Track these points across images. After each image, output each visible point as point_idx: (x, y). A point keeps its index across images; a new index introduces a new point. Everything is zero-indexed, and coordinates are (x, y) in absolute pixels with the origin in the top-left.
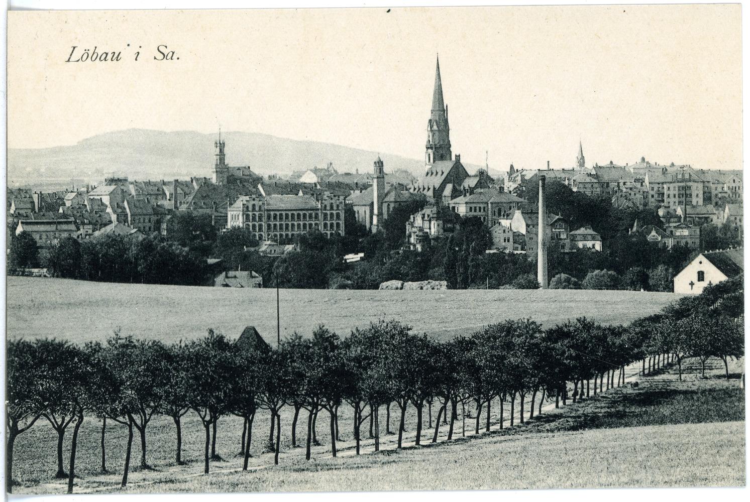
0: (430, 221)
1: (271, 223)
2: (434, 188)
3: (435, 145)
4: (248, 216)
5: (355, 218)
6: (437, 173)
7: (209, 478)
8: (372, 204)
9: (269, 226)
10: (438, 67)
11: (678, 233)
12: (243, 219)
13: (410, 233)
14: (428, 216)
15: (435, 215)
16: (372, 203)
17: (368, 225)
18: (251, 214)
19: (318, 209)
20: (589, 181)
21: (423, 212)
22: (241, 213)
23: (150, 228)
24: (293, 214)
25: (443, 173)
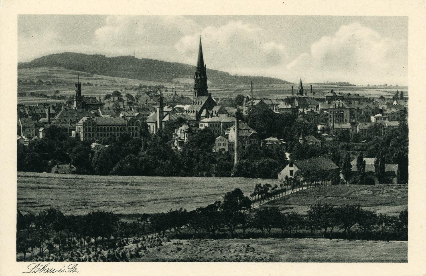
0: (184, 133)
1: (99, 132)
2: (197, 111)
3: (198, 87)
4: (86, 128)
5: (148, 129)
6: (199, 103)
7: (292, 85)
8: (156, 123)
9: (98, 134)
10: (201, 41)
11: (237, 86)
12: (83, 130)
13: (174, 140)
14: (184, 130)
15: (187, 130)
16: (157, 122)
17: (201, 121)
18: (88, 127)
19: (125, 125)
20: (286, 108)
21: (181, 128)
22: (82, 127)
23: (33, 134)
24: (101, 128)
25: (202, 103)
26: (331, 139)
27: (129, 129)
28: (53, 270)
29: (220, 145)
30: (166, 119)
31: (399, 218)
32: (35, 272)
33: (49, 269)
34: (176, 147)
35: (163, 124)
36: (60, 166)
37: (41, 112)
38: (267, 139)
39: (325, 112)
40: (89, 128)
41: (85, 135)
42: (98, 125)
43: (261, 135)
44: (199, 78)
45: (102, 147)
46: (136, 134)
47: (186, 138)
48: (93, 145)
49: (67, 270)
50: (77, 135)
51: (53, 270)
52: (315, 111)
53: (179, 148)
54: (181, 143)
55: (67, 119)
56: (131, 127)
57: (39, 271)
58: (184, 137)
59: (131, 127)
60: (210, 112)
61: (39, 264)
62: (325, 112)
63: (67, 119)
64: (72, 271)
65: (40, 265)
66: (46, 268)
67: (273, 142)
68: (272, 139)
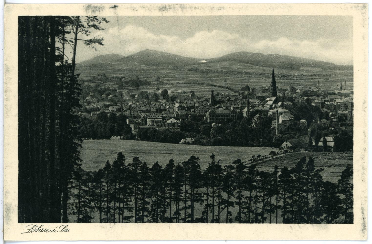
19: (230, 114)
26: (335, 120)
27: (232, 116)
28: (47, 230)
29: (273, 125)
30: (251, 110)
31: (146, 206)
32: (32, 231)
33: (43, 229)
34: (253, 125)
35: (249, 113)
36: (187, 139)
37: (192, 106)
38: (301, 121)
39: (339, 104)
40: (212, 116)
41: (210, 119)
42: (216, 114)
43: (297, 118)
44: (272, 87)
45: (217, 125)
46: (235, 118)
47: (258, 121)
48: (213, 124)
49: (59, 230)
50: (206, 119)
51: (47, 230)
52: (334, 103)
53: (255, 126)
54: (256, 123)
55: (203, 110)
56: (233, 115)
57: (35, 231)
58: (257, 120)
59: (233, 115)
60: (277, 105)
61: (36, 225)
62: (339, 104)
63: (203, 110)
64: (64, 230)
65: (36, 226)
66: (40, 229)
67: (303, 122)
68: (303, 121)
